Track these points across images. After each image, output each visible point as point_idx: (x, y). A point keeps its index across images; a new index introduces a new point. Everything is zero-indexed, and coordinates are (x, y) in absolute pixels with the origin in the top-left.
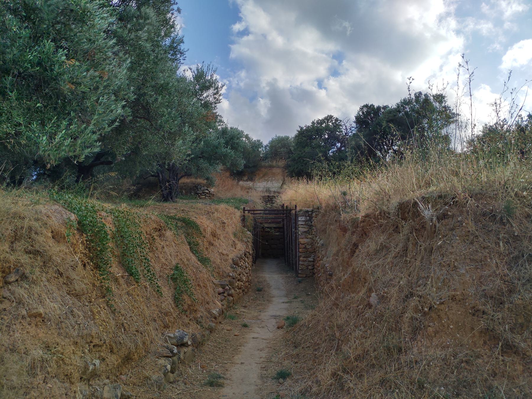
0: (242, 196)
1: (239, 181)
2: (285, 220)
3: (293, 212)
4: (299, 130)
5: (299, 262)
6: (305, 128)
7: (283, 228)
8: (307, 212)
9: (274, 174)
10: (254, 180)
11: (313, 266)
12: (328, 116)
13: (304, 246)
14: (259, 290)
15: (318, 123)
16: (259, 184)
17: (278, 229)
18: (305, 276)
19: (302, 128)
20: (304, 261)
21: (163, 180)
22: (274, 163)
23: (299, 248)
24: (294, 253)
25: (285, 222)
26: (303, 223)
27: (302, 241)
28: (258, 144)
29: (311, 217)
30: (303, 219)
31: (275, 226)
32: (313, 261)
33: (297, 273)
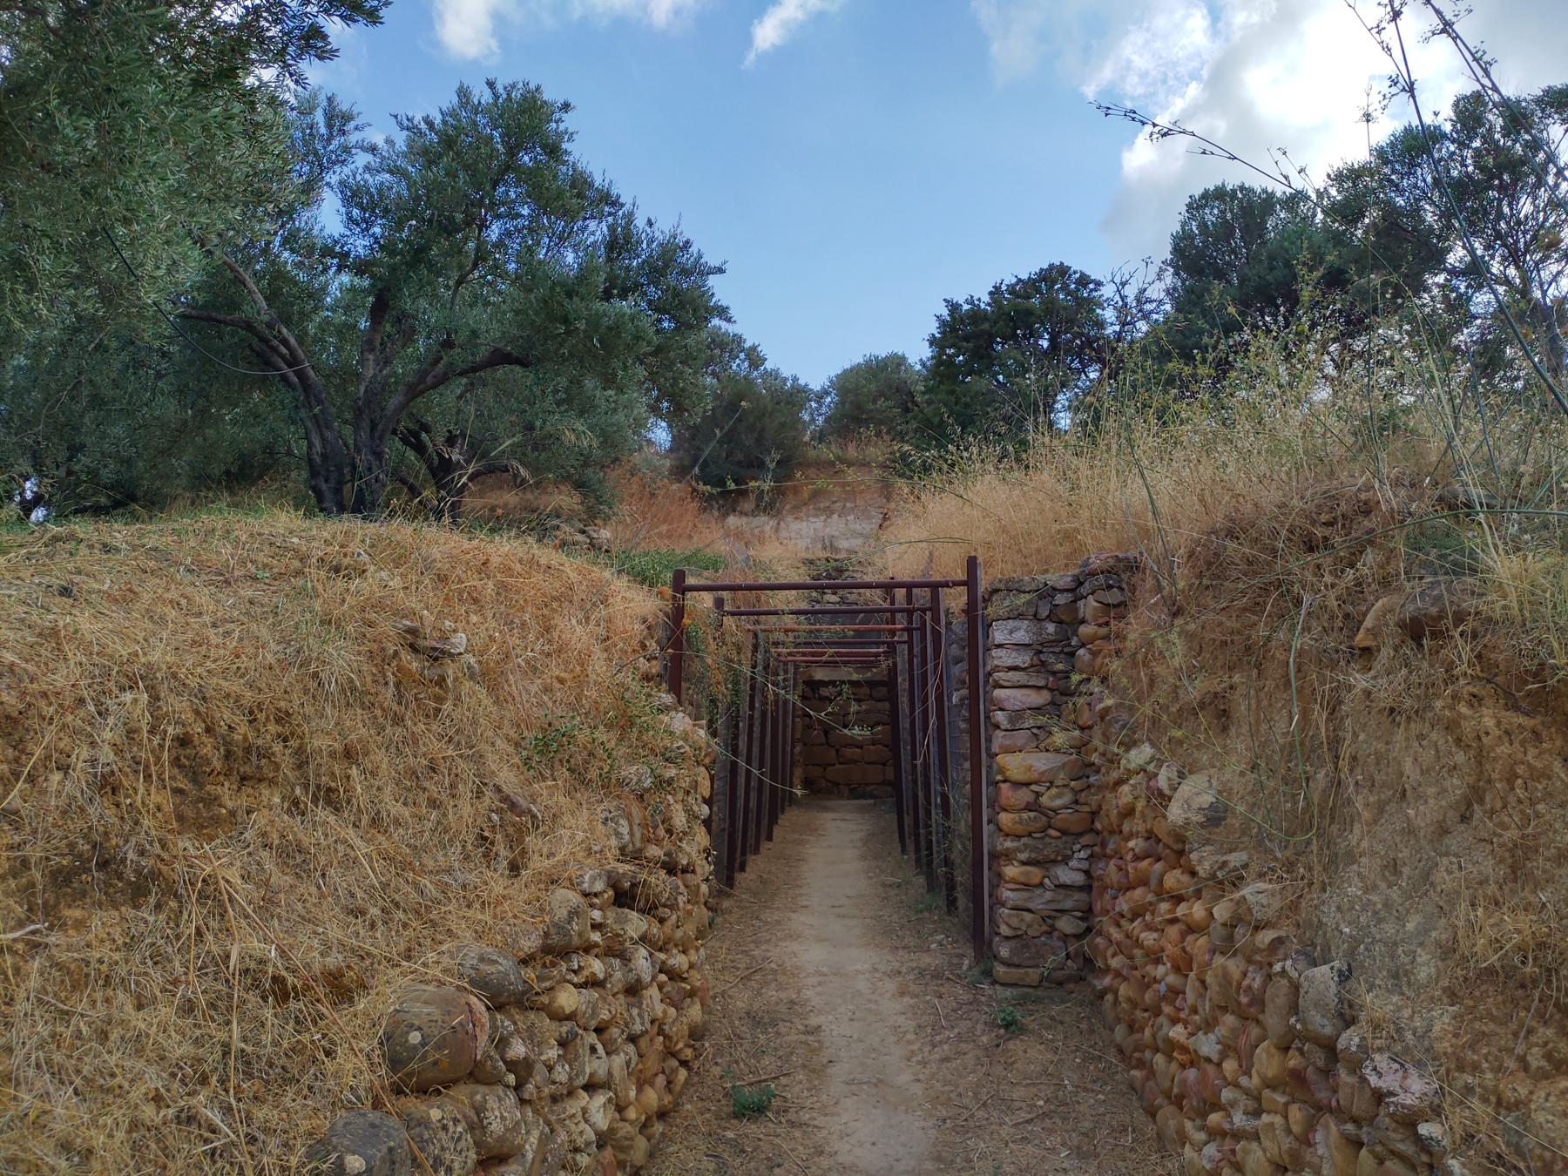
0: (1029, 768)
1: (725, 516)
3: (954, 600)
4: (945, 312)
5: (994, 887)
6: (966, 307)
7: (890, 683)
9: (851, 493)
10: (779, 512)
11: (1088, 912)
12: (1051, 267)
13: (1025, 796)
14: (753, 1110)
15: (1012, 289)
16: (795, 526)
19: (954, 307)
20: (1027, 886)
21: (324, 457)
22: (852, 452)
23: (996, 806)
24: (963, 824)
25: (901, 660)
26: (1023, 659)
27: (1014, 764)
28: (794, 397)
29: (1069, 621)
30: (1021, 636)
31: (855, 677)
32: (1086, 888)
33: (979, 936)
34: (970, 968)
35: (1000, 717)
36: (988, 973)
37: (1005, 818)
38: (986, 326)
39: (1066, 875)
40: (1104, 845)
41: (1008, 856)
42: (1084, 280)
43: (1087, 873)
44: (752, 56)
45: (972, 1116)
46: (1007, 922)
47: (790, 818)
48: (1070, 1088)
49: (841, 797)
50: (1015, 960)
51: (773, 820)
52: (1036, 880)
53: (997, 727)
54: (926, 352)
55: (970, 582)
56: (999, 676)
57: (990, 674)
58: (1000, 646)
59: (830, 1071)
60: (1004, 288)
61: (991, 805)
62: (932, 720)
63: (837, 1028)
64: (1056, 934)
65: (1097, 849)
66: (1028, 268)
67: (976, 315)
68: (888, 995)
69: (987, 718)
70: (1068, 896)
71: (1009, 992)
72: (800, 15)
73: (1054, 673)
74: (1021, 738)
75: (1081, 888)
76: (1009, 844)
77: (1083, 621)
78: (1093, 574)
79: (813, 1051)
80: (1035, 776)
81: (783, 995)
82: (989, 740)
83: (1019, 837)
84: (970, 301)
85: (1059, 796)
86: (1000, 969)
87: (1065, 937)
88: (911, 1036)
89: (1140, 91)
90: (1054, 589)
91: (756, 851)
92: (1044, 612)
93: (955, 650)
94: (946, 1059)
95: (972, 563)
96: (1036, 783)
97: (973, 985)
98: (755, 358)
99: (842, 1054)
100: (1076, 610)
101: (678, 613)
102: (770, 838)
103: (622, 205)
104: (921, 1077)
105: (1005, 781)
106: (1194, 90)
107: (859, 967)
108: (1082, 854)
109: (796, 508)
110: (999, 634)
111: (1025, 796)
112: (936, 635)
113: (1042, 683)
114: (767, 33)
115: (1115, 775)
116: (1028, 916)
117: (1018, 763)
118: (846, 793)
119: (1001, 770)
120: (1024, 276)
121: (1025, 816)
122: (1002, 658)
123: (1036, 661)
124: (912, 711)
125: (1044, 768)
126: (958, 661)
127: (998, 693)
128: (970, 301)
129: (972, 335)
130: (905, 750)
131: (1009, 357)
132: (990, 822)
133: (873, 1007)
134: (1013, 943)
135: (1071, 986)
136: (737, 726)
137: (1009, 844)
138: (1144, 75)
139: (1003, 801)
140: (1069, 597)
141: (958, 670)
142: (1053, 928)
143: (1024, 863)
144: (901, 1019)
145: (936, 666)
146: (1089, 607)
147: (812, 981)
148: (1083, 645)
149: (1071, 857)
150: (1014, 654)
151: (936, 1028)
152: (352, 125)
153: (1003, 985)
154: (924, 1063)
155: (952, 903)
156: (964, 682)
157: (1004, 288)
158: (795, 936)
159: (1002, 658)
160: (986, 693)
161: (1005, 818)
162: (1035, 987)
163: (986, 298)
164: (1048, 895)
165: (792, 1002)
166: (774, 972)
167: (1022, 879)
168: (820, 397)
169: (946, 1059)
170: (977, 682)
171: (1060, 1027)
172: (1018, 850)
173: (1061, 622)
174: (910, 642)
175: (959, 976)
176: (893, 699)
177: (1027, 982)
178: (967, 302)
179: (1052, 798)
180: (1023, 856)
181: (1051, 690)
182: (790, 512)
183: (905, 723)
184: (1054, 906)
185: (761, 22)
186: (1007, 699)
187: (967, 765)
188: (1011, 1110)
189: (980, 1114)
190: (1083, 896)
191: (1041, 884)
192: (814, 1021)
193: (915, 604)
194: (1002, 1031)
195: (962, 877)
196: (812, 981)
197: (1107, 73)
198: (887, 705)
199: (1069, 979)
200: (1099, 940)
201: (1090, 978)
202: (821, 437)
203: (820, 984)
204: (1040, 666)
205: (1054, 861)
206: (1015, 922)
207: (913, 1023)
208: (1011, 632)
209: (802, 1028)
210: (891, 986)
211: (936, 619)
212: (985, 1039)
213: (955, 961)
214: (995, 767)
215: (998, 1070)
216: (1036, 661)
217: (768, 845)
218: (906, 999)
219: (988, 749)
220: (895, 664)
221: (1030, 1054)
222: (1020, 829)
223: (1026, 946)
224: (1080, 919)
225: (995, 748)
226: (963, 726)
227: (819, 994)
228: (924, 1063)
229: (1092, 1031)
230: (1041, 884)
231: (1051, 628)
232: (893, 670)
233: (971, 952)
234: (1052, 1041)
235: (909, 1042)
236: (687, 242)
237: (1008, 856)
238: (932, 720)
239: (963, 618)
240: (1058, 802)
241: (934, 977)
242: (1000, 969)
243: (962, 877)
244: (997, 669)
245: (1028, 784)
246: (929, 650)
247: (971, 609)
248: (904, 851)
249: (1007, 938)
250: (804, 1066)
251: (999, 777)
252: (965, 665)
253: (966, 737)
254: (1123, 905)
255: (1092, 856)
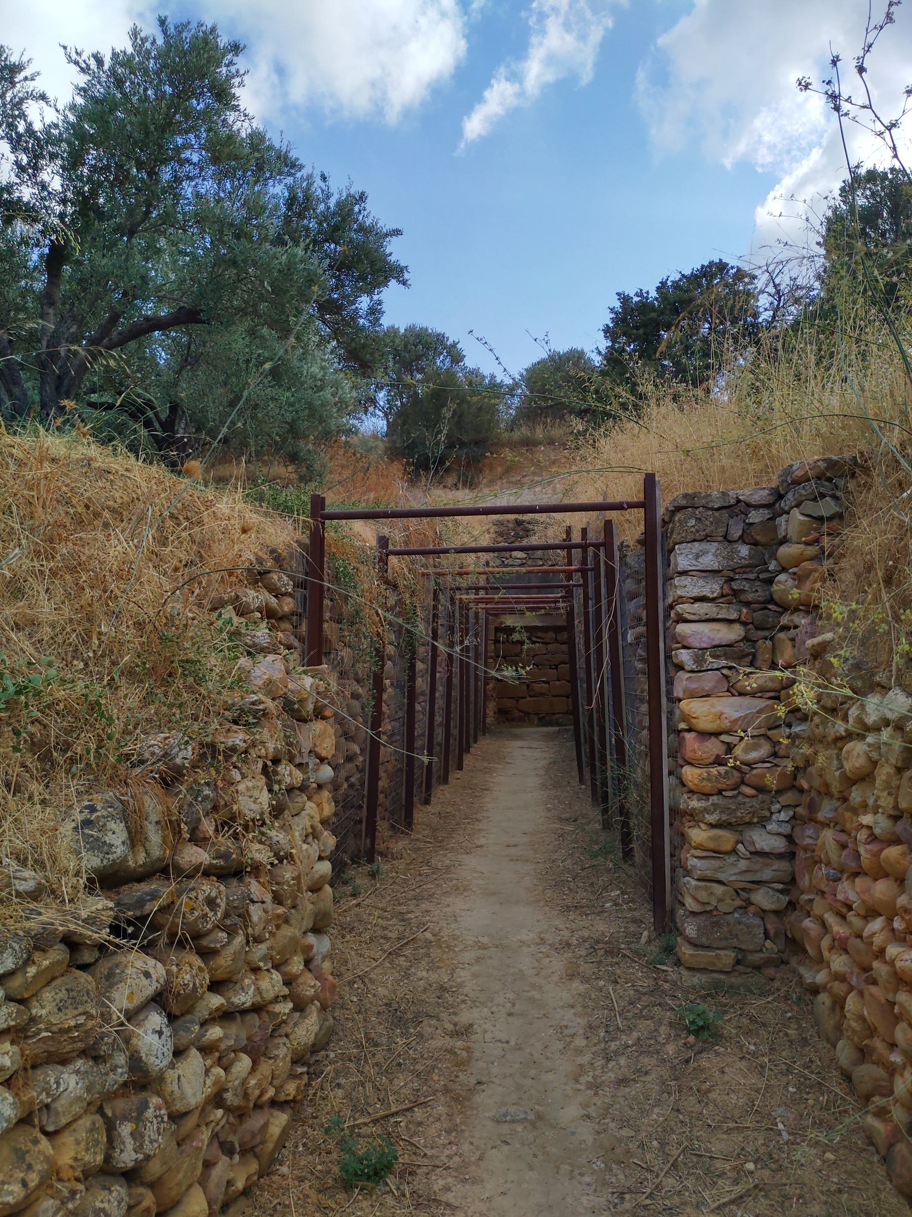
0: (720, 716)
2: (579, 593)
3: (630, 529)
4: (617, 305)
6: (636, 299)
7: (569, 627)
8: (738, 508)
11: (791, 883)
12: (711, 264)
13: (713, 747)
14: (367, 1174)
15: (676, 285)
17: (551, 635)
18: (727, 957)
19: (625, 299)
20: (717, 853)
24: (640, 771)
26: (711, 588)
27: (701, 711)
29: (766, 542)
30: (709, 561)
32: (790, 856)
33: (659, 895)
34: (649, 941)
35: (684, 656)
36: (669, 950)
37: (690, 773)
38: (654, 315)
39: (764, 840)
40: (812, 807)
41: (693, 816)
42: (740, 275)
43: (789, 838)
44: (462, 145)
45: (659, 1187)
46: (692, 894)
47: (484, 745)
48: (785, 1136)
49: (531, 724)
50: (704, 940)
51: (464, 749)
52: (728, 847)
53: (680, 667)
54: (604, 344)
55: (648, 503)
56: (684, 608)
57: (671, 607)
58: (684, 573)
59: (478, 1099)
60: (669, 284)
61: (673, 755)
62: (606, 659)
63: (491, 1027)
64: (752, 909)
65: (800, 810)
66: (690, 264)
67: (644, 306)
68: (555, 978)
69: (668, 657)
70: (767, 865)
71: (697, 979)
72: (502, 112)
73: (748, 604)
74: (709, 680)
75: (780, 856)
76: (695, 803)
77: (784, 541)
78: (797, 482)
79: (461, 1064)
80: (726, 724)
81: (433, 977)
82: (670, 682)
83: (707, 795)
84: (640, 294)
85: (755, 747)
86: (686, 951)
87: (762, 913)
88: (580, 1042)
89: (769, 159)
90: (748, 505)
91: (445, 780)
92: (736, 532)
93: (630, 585)
94: (623, 1082)
95: (650, 481)
96: (727, 732)
97: (652, 966)
98: (456, 357)
99: (495, 1070)
100: (775, 529)
101: (316, 547)
102: (460, 768)
103: (301, 167)
104: (592, 1111)
105: (689, 730)
106: (816, 154)
107: (524, 937)
108: (783, 816)
109: (492, 482)
110: (683, 559)
111: (713, 747)
112: (610, 571)
113: (734, 616)
114: (475, 125)
115: (840, 728)
116: (719, 889)
117: (707, 709)
118: (536, 722)
119: (685, 718)
120: (687, 272)
121: (714, 771)
122: (688, 587)
123: (726, 590)
124: (587, 648)
125: (736, 715)
126: (633, 596)
127: (682, 628)
128: (640, 294)
129: (642, 325)
130: (582, 688)
131: (677, 328)
132: (670, 773)
133: (535, 994)
134: (701, 920)
135: (771, 971)
136: (412, 667)
137: (695, 803)
138: (772, 147)
139: (689, 755)
140: (765, 514)
141: (635, 607)
142: (749, 902)
143: (712, 826)
144: (569, 1014)
145: (610, 603)
146: (794, 522)
147: (468, 956)
148: (784, 570)
149: (769, 819)
150: (701, 582)
151: (612, 1033)
152: (19, 77)
153: (689, 969)
154: (595, 1086)
155: (628, 854)
156: (640, 619)
157: (669, 284)
158: (461, 889)
159: (688, 587)
160: (666, 629)
161: (690, 773)
162: (726, 973)
163: (653, 294)
164: (743, 864)
165: (443, 989)
166: (428, 943)
167: (711, 845)
168: (512, 390)
169: (623, 1082)
170: (656, 619)
171: (762, 1032)
172: (706, 810)
173: (756, 544)
174: (585, 586)
175: (637, 953)
176: (571, 642)
177: (719, 966)
178: (637, 295)
179: (746, 751)
180: (712, 818)
181: (744, 624)
182: (487, 486)
183: (580, 663)
184: (749, 877)
185: (469, 117)
186: (695, 633)
187: (644, 708)
188: (712, 1176)
189: (670, 1182)
190: (782, 866)
191: (734, 851)
192: (465, 1017)
193: (593, 557)
194: (692, 1039)
195: (640, 829)
196: (468, 956)
197: (742, 147)
198: (565, 648)
199: (768, 963)
200: (807, 923)
201: (794, 961)
202: (513, 425)
203: (478, 960)
204: (733, 596)
205: (750, 824)
206: (703, 896)
207: (583, 1021)
208: (697, 557)
209: (450, 1027)
210: (558, 964)
211: (610, 555)
212: (671, 1049)
213: (632, 928)
214: (677, 712)
215: (690, 1103)
216: (726, 590)
217: (458, 774)
218: (576, 984)
219: (669, 692)
220: (572, 608)
221: (730, 1075)
222: (708, 786)
223: (717, 924)
224: (781, 892)
225: (678, 692)
226: (639, 665)
227: (475, 976)
228: (595, 1086)
229: (805, 1042)
230: (734, 851)
231: (744, 550)
232: (570, 615)
233: (649, 918)
234: (754, 1054)
235: (579, 1052)
236: (363, 194)
237: (693, 816)
238: (606, 659)
239: (640, 550)
240: (754, 755)
241: (609, 953)
242: (686, 951)
243: (640, 829)
244: (680, 600)
245: (717, 734)
246: (603, 590)
247: (648, 541)
248: (582, 780)
249: (693, 913)
250: (446, 1090)
251: (682, 726)
252: (642, 600)
253: (643, 679)
254: (847, 891)
255: (794, 817)
